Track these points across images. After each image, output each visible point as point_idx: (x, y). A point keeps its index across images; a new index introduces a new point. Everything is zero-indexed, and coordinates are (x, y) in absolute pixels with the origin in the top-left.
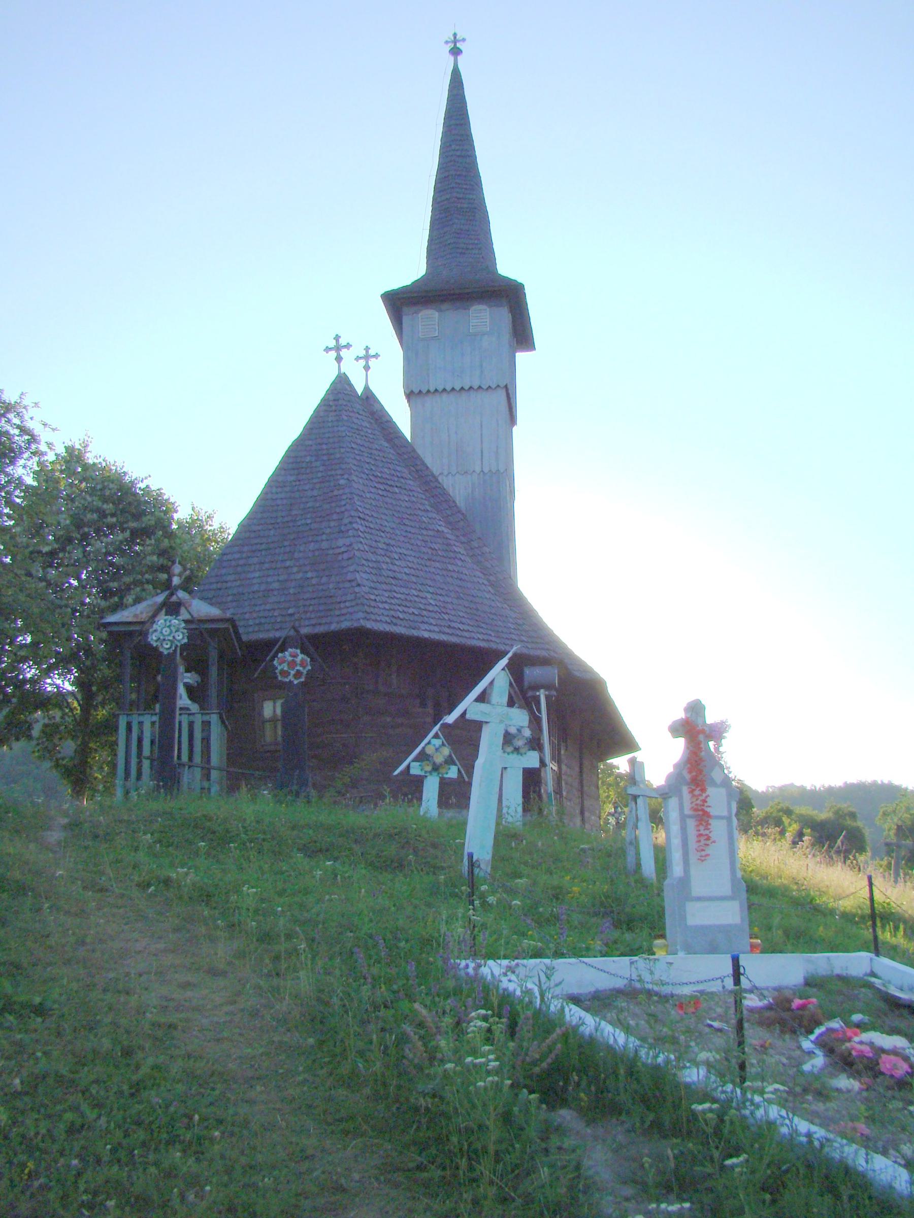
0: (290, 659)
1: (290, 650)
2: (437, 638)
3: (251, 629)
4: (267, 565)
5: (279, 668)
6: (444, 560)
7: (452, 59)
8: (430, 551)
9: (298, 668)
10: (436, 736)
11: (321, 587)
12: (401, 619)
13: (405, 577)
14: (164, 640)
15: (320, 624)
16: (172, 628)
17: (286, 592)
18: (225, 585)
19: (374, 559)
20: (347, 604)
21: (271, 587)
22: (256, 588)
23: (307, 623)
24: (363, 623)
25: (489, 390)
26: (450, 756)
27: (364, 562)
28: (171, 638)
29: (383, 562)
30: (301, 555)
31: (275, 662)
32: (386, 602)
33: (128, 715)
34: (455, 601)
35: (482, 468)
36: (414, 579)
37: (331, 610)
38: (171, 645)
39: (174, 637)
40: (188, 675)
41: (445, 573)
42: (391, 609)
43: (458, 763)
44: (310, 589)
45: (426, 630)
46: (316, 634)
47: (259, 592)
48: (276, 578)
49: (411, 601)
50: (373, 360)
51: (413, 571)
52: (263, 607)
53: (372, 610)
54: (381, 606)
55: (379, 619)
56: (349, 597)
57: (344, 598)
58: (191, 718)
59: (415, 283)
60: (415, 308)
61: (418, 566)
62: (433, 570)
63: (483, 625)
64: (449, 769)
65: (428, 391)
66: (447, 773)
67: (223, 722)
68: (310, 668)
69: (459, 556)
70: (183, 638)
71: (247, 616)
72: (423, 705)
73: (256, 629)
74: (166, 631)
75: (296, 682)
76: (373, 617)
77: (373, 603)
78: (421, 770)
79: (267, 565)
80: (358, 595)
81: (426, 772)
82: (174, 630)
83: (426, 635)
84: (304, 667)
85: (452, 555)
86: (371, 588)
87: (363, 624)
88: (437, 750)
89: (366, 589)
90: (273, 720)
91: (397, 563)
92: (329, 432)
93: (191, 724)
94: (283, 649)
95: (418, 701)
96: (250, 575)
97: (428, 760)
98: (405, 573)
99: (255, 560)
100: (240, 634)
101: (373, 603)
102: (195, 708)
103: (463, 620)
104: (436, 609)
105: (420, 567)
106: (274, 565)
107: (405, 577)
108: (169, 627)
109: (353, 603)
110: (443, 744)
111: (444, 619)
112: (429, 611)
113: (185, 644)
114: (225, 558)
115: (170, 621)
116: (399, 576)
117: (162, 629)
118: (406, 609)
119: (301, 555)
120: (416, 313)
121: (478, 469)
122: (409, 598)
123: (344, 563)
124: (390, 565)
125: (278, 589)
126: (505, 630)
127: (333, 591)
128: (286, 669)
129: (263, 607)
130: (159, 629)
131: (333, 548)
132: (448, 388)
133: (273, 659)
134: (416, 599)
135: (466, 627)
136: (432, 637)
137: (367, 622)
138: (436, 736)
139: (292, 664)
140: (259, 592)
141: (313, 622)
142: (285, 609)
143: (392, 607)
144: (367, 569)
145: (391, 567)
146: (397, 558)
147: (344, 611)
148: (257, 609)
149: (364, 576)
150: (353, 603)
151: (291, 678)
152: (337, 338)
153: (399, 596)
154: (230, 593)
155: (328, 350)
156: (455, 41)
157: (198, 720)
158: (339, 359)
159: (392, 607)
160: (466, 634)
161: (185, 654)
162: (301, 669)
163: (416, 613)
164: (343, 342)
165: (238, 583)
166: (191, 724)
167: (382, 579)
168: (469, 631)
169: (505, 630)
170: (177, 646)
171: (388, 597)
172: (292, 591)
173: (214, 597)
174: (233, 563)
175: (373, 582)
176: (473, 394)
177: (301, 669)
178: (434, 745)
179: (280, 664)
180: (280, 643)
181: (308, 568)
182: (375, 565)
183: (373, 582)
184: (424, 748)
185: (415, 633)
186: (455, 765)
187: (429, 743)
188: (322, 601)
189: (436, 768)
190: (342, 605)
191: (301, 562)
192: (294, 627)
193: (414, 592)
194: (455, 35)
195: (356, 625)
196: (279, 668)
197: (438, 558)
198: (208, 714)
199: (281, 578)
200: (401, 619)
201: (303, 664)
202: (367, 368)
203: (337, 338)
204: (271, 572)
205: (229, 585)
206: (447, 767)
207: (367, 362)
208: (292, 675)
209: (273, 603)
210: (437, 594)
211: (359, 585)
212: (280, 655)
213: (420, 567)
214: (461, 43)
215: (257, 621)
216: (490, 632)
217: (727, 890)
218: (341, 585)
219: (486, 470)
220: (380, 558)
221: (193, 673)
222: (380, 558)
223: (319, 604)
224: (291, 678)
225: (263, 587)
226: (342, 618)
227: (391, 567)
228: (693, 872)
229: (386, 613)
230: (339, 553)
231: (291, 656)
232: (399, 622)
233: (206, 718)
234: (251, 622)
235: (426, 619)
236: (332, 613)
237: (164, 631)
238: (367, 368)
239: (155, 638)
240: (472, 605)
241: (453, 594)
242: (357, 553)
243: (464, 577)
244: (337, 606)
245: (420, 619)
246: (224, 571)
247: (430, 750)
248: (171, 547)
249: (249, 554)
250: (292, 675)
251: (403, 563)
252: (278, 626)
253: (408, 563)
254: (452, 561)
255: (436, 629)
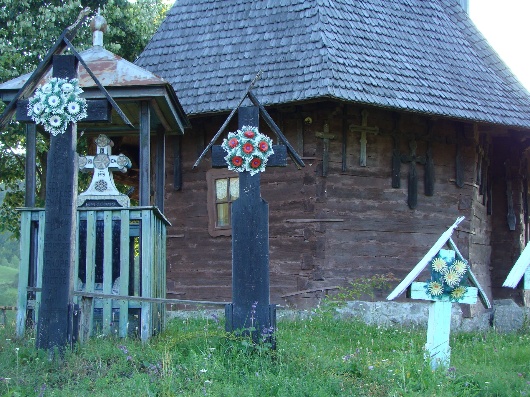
0: (244, 140)
1: (244, 127)
2: (416, 108)
3: (200, 100)
4: (217, 27)
5: (230, 153)
6: (420, 18)
8: (403, 8)
9: (256, 153)
10: (448, 246)
11: (280, 50)
12: (375, 86)
13: (376, 37)
14: (51, 114)
15: (280, 93)
16: (63, 96)
17: (240, 56)
18: (171, 50)
19: (341, 17)
20: (312, 69)
21: (223, 52)
22: (206, 52)
23: (264, 91)
26: (467, 273)
27: (330, 20)
28: (61, 111)
29: (352, 20)
30: (256, 13)
31: (224, 145)
32: (356, 66)
33: (32, 212)
34: (434, 65)
36: (387, 40)
37: (291, 76)
38: (63, 123)
39: (66, 110)
40: (116, 157)
41: (420, 32)
42: (361, 75)
43: (477, 283)
44: (268, 52)
45: (403, 98)
46: (276, 105)
47: (210, 56)
48: (227, 41)
49: (384, 65)
51: (385, 31)
52: (213, 75)
53: (341, 75)
54: (351, 70)
55: (348, 86)
56: (314, 61)
57: (308, 62)
58: (117, 215)
61: (390, 25)
62: (408, 29)
63: (467, 92)
64: (466, 291)
66: (462, 298)
67: (159, 217)
68: (272, 152)
69: (436, 13)
70: (81, 111)
71: (196, 85)
72: (396, 185)
73: (207, 98)
74: (54, 101)
75: (253, 173)
76: (343, 84)
77: (341, 68)
78: (428, 292)
79: (217, 27)
80: (323, 57)
81: (433, 296)
82: (65, 100)
83: (404, 104)
84: (265, 153)
85: (429, 12)
86: (338, 49)
87: (331, 93)
88: (449, 265)
89: (333, 52)
90: (228, 201)
91: (366, 20)
92: (250, 73)
93: (117, 225)
94: (234, 127)
95: (390, 180)
96: (200, 38)
97: (435, 280)
98: (377, 33)
99: (205, 21)
100: (181, 106)
101: (341, 68)
102: (124, 200)
103: (445, 87)
104: (413, 74)
105: (393, 26)
106: (226, 26)
107: (376, 37)
108: (58, 94)
109: (319, 68)
110: (457, 257)
111: (423, 85)
112: (406, 76)
113: (84, 121)
114: (172, 19)
115: (60, 86)
116: (368, 35)
117: (47, 99)
118: (379, 75)
119: (256, 13)
122: (382, 61)
123: (307, 22)
124: (360, 23)
125: (232, 54)
126: (493, 98)
127: (294, 54)
128: (239, 154)
129: (213, 75)
130: (43, 98)
131: (294, 5)
133: (220, 141)
134: (391, 63)
135: (448, 95)
136: (411, 107)
137: (335, 89)
138: (448, 246)
139: (248, 148)
140: (210, 56)
141: (272, 90)
142: (239, 75)
143: (364, 72)
144: (333, 28)
145: (360, 25)
146: (367, 15)
147: (307, 78)
148: (208, 76)
149: (331, 36)
150: (319, 68)
151: (246, 167)
153: (370, 59)
154: (177, 58)
157: (125, 218)
159: (364, 72)
160: (448, 103)
161: (82, 133)
162: (260, 154)
163: (392, 79)
165: (187, 47)
166: (117, 225)
167: (351, 40)
168: (452, 99)
169: (493, 98)
170: (71, 124)
171: (359, 61)
172: (246, 55)
173: (159, 63)
174: (181, 25)
175: (340, 43)
177: (260, 154)
178: (445, 258)
179: (231, 148)
180: (229, 118)
181: (265, 29)
182: (342, 23)
183: (340, 43)
184: (430, 263)
185: (391, 102)
186: (474, 285)
187: (437, 256)
188: (282, 66)
189: (448, 291)
190: (305, 71)
191: (258, 21)
192: (249, 95)
193: (388, 54)
195: (322, 93)
196: (230, 153)
197: (413, 16)
198: (141, 210)
199: (235, 40)
200: (375, 86)
201: (262, 147)
204: (223, 34)
205: (176, 49)
206: (464, 289)
208: (247, 163)
209: (196, 11)
210: (413, 57)
211: (324, 46)
212: (230, 135)
213: (393, 26)
215: (208, 90)
216: (476, 101)
218: (303, 47)
220: (348, 16)
221: (121, 155)
222: (348, 16)
223: (279, 70)
224: (246, 167)
225: (214, 51)
226: (306, 85)
227: (360, 25)
229: (356, 79)
230: (301, 10)
231: (246, 136)
232: (373, 90)
233: (136, 215)
234: (200, 92)
235: (402, 86)
236: (294, 80)
237: (50, 101)
239: (37, 112)
240: (454, 70)
241: (431, 57)
242: (321, 9)
243: (442, 37)
244: (300, 72)
245: (395, 86)
246: (170, 34)
247: (439, 266)
248: (125, 17)
249: (198, 14)
250: (247, 163)
251: (374, 22)
252: (230, 96)
253: (379, 21)
254: (428, 19)
255: (415, 98)
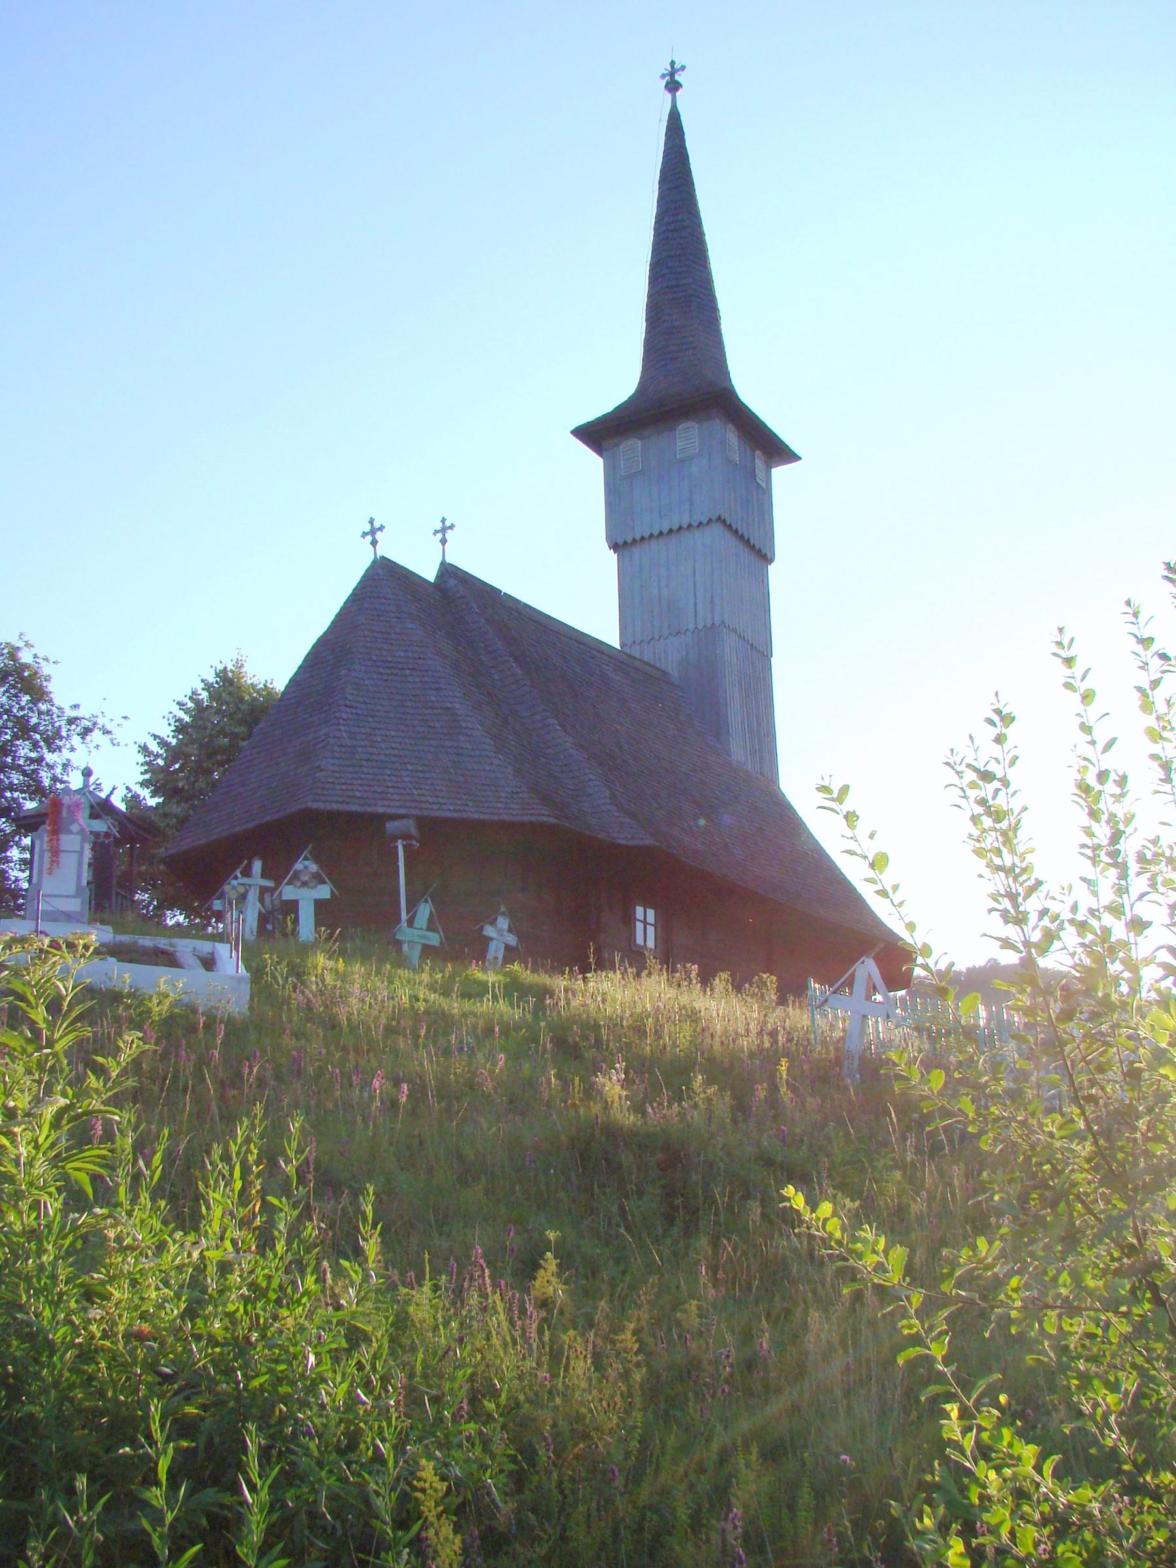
7: (669, 96)
24: (309, 804)
25: (701, 527)
35: (696, 625)
50: (449, 531)
59: (632, 399)
60: (616, 441)
65: (634, 540)
120: (617, 445)
121: (691, 627)
132: (647, 535)
152: (371, 522)
155: (365, 535)
156: (672, 74)
158: (374, 543)
164: (377, 525)
176: (654, 542)
194: (672, 63)
202: (444, 541)
203: (371, 522)
207: (444, 535)
214: (680, 73)
217: (72, 890)
219: (700, 627)
228: (44, 881)
238: (444, 541)
